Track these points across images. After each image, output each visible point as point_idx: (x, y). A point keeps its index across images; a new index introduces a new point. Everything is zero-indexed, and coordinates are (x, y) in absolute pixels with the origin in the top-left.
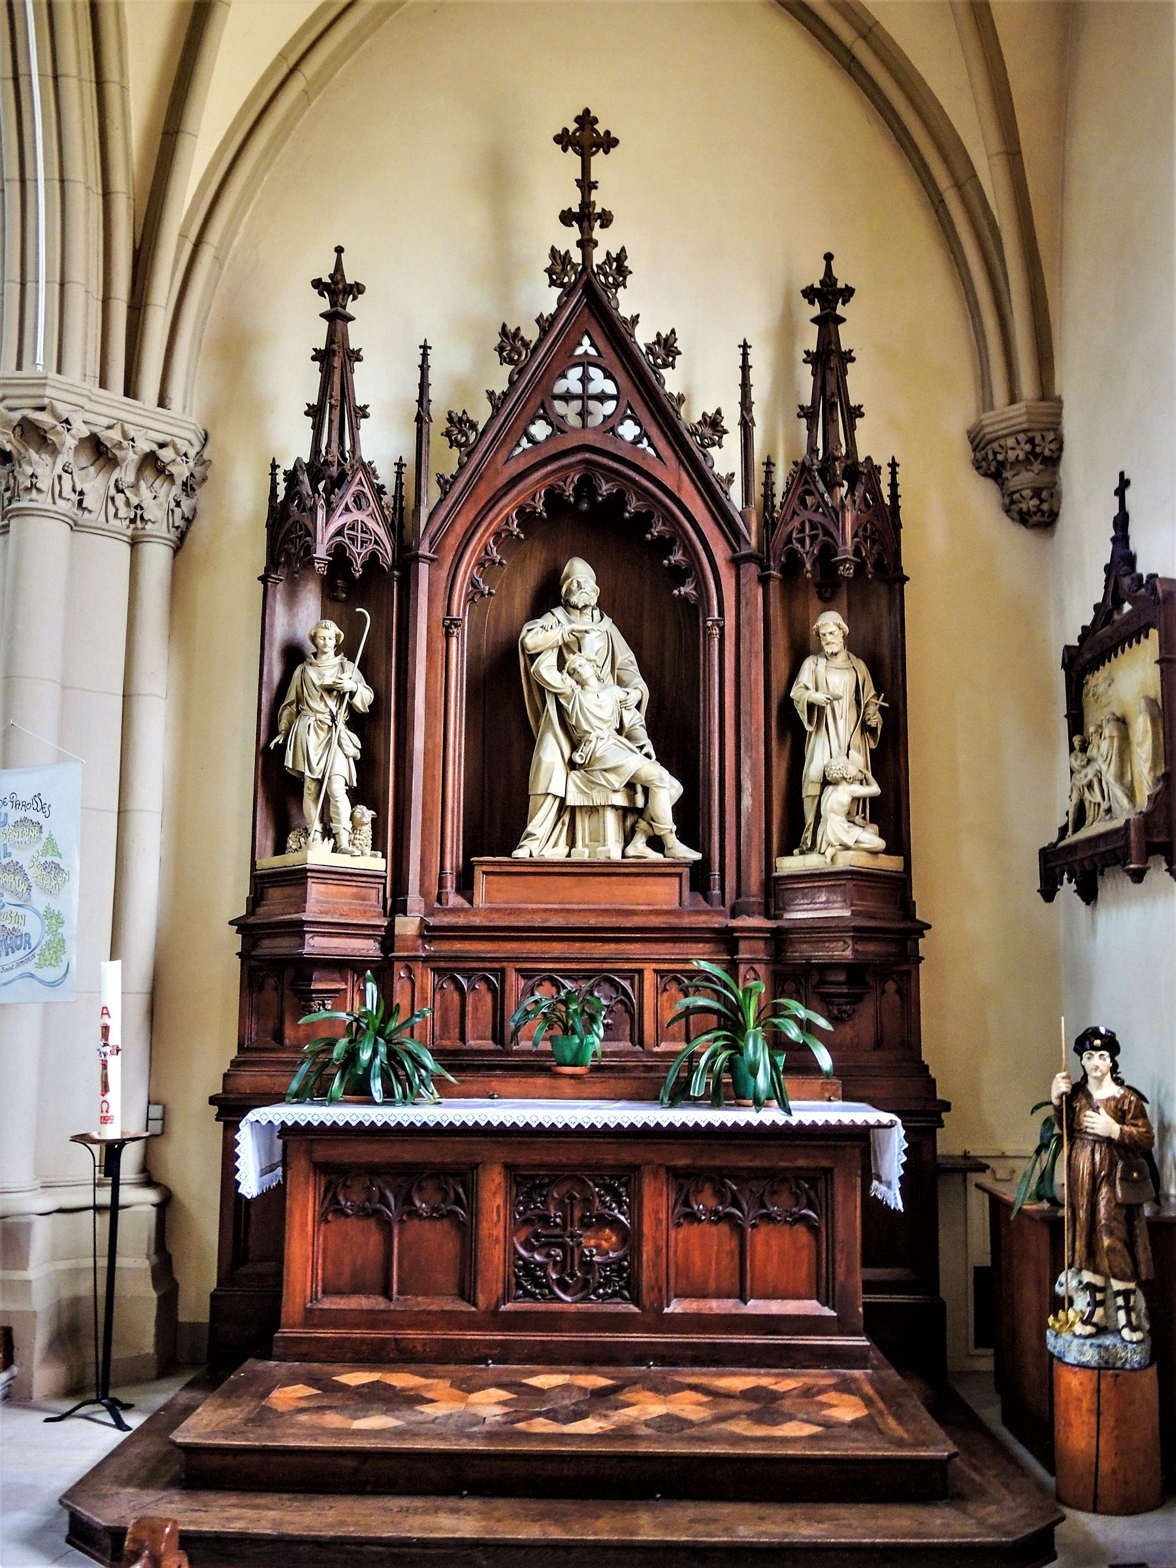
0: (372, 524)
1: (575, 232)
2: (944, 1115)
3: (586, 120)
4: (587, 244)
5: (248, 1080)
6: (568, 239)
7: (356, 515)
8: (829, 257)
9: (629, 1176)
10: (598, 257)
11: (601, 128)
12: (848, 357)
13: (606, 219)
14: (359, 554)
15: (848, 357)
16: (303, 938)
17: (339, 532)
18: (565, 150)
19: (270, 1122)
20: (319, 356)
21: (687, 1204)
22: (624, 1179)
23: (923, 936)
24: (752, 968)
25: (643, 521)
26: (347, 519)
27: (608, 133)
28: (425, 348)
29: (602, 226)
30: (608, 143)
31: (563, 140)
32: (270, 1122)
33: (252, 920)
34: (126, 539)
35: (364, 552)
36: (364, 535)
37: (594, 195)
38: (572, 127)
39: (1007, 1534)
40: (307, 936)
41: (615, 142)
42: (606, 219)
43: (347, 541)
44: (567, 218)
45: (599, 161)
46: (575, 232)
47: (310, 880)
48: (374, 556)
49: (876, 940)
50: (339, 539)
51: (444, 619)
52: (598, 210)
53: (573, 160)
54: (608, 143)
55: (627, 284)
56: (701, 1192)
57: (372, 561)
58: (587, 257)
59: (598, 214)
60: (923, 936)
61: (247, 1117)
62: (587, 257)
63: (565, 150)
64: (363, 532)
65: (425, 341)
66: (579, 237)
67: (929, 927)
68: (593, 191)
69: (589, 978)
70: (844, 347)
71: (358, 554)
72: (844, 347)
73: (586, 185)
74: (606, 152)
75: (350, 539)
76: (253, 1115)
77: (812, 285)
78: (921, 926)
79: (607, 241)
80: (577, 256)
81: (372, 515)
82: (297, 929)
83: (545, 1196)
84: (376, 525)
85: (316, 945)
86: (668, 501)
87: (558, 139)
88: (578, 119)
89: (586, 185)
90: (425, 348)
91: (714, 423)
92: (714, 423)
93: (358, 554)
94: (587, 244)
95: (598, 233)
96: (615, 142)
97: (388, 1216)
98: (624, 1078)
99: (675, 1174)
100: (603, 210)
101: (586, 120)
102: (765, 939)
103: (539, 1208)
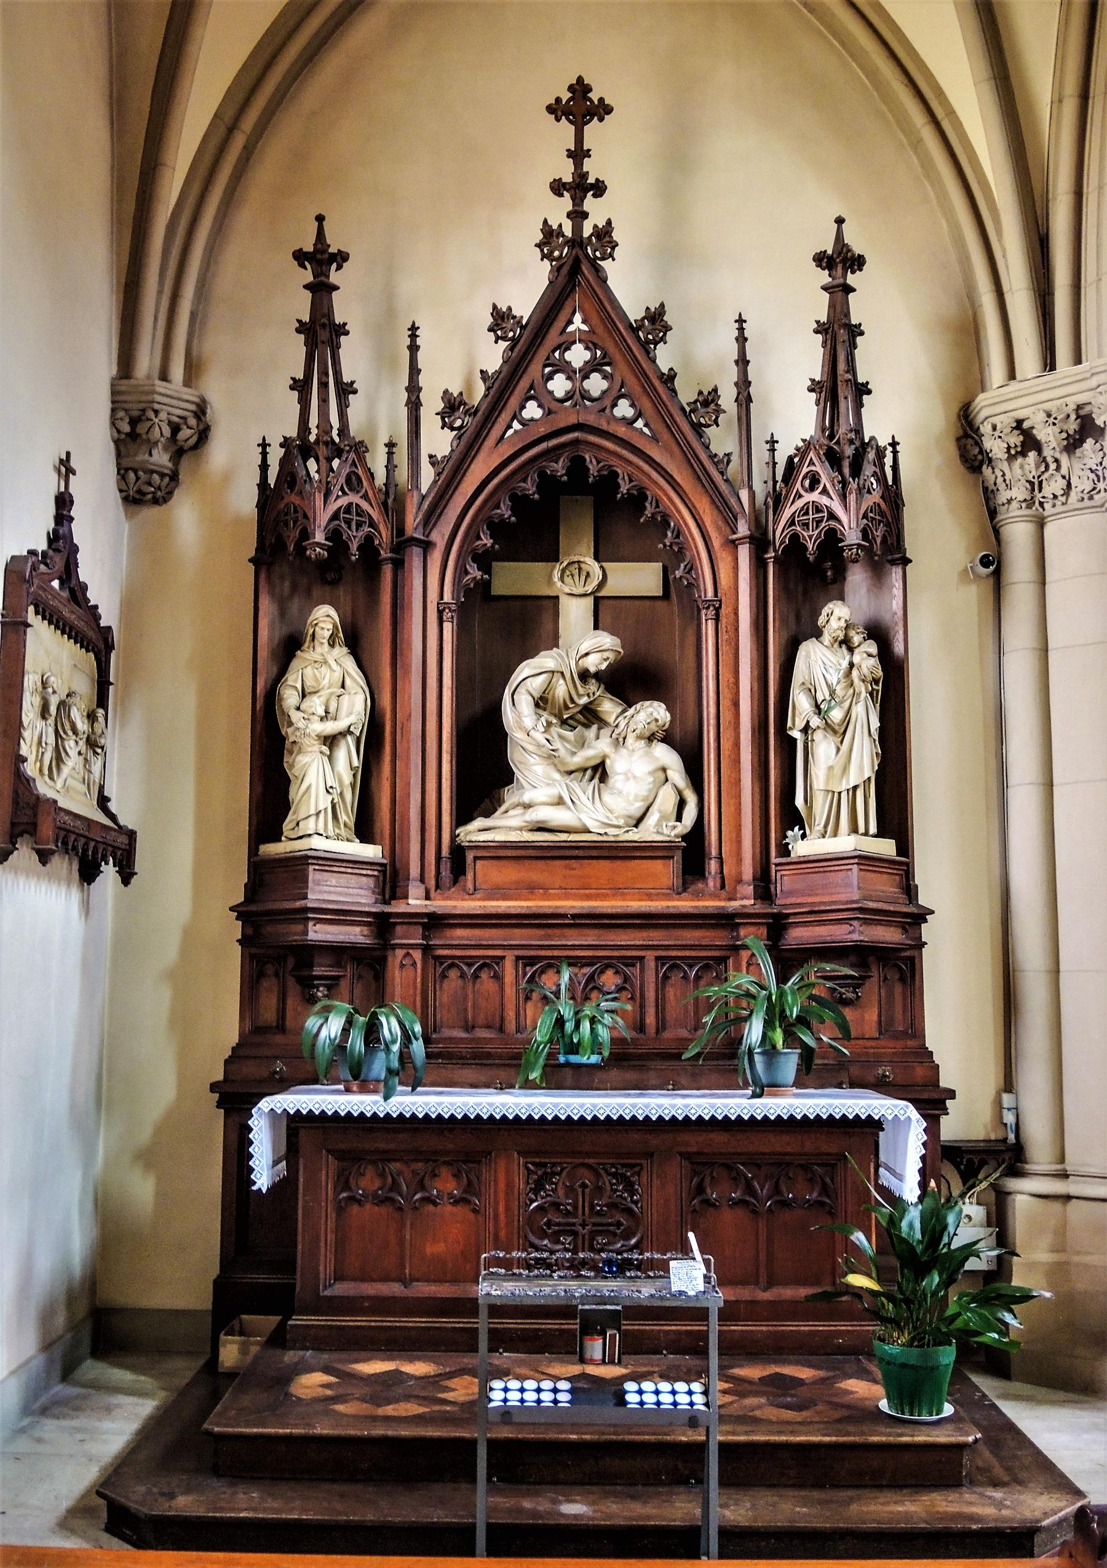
0: (365, 505)
1: (566, 203)
2: (949, 1103)
3: (580, 89)
4: (578, 215)
5: (251, 1070)
6: (558, 210)
7: (815, 496)
8: (840, 221)
9: (641, 1165)
10: (587, 231)
11: (594, 96)
12: (341, 330)
13: (599, 189)
14: (354, 537)
15: (341, 330)
16: (306, 926)
17: (335, 516)
18: (558, 120)
19: (272, 1109)
20: (821, 329)
21: (700, 1189)
22: (637, 1169)
23: (926, 921)
24: (408, 954)
25: (519, 503)
26: (343, 501)
27: (601, 100)
28: (741, 321)
29: (595, 196)
30: (603, 110)
31: (556, 110)
32: (272, 1109)
33: (253, 908)
34: (1049, 519)
35: (360, 534)
36: (358, 518)
37: (588, 165)
38: (566, 96)
39: (930, 1524)
40: (311, 924)
41: (609, 110)
42: (599, 189)
43: (343, 524)
44: (558, 188)
45: (593, 131)
46: (566, 203)
47: (311, 868)
48: (369, 538)
49: (888, 924)
50: (337, 522)
51: (438, 604)
52: (591, 180)
53: (566, 130)
54: (603, 110)
55: (615, 255)
56: (363, 1175)
57: (368, 546)
58: (577, 229)
59: (591, 184)
60: (926, 921)
61: (259, 1105)
62: (577, 229)
63: (558, 120)
64: (807, 513)
65: (740, 314)
66: (570, 208)
67: (932, 912)
68: (586, 160)
69: (592, 965)
70: (338, 320)
71: (355, 540)
72: (338, 320)
73: (578, 154)
74: (601, 120)
75: (345, 522)
76: (266, 1104)
77: (826, 251)
78: (927, 912)
79: (597, 211)
80: (568, 231)
81: (365, 497)
82: (302, 915)
83: (556, 1184)
84: (370, 507)
85: (318, 933)
86: (496, 481)
87: (550, 109)
88: (571, 88)
89: (578, 154)
90: (741, 321)
91: (709, 400)
92: (709, 400)
93: (355, 540)
94: (578, 215)
95: (590, 203)
96: (609, 110)
97: (400, 1203)
98: (475, 1064)
99: (341, 1155)
100: (597, 180)
101: (580, 89)
102: (768, 924)
103: (550, 1195)
